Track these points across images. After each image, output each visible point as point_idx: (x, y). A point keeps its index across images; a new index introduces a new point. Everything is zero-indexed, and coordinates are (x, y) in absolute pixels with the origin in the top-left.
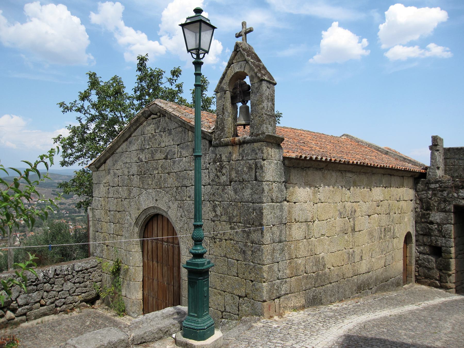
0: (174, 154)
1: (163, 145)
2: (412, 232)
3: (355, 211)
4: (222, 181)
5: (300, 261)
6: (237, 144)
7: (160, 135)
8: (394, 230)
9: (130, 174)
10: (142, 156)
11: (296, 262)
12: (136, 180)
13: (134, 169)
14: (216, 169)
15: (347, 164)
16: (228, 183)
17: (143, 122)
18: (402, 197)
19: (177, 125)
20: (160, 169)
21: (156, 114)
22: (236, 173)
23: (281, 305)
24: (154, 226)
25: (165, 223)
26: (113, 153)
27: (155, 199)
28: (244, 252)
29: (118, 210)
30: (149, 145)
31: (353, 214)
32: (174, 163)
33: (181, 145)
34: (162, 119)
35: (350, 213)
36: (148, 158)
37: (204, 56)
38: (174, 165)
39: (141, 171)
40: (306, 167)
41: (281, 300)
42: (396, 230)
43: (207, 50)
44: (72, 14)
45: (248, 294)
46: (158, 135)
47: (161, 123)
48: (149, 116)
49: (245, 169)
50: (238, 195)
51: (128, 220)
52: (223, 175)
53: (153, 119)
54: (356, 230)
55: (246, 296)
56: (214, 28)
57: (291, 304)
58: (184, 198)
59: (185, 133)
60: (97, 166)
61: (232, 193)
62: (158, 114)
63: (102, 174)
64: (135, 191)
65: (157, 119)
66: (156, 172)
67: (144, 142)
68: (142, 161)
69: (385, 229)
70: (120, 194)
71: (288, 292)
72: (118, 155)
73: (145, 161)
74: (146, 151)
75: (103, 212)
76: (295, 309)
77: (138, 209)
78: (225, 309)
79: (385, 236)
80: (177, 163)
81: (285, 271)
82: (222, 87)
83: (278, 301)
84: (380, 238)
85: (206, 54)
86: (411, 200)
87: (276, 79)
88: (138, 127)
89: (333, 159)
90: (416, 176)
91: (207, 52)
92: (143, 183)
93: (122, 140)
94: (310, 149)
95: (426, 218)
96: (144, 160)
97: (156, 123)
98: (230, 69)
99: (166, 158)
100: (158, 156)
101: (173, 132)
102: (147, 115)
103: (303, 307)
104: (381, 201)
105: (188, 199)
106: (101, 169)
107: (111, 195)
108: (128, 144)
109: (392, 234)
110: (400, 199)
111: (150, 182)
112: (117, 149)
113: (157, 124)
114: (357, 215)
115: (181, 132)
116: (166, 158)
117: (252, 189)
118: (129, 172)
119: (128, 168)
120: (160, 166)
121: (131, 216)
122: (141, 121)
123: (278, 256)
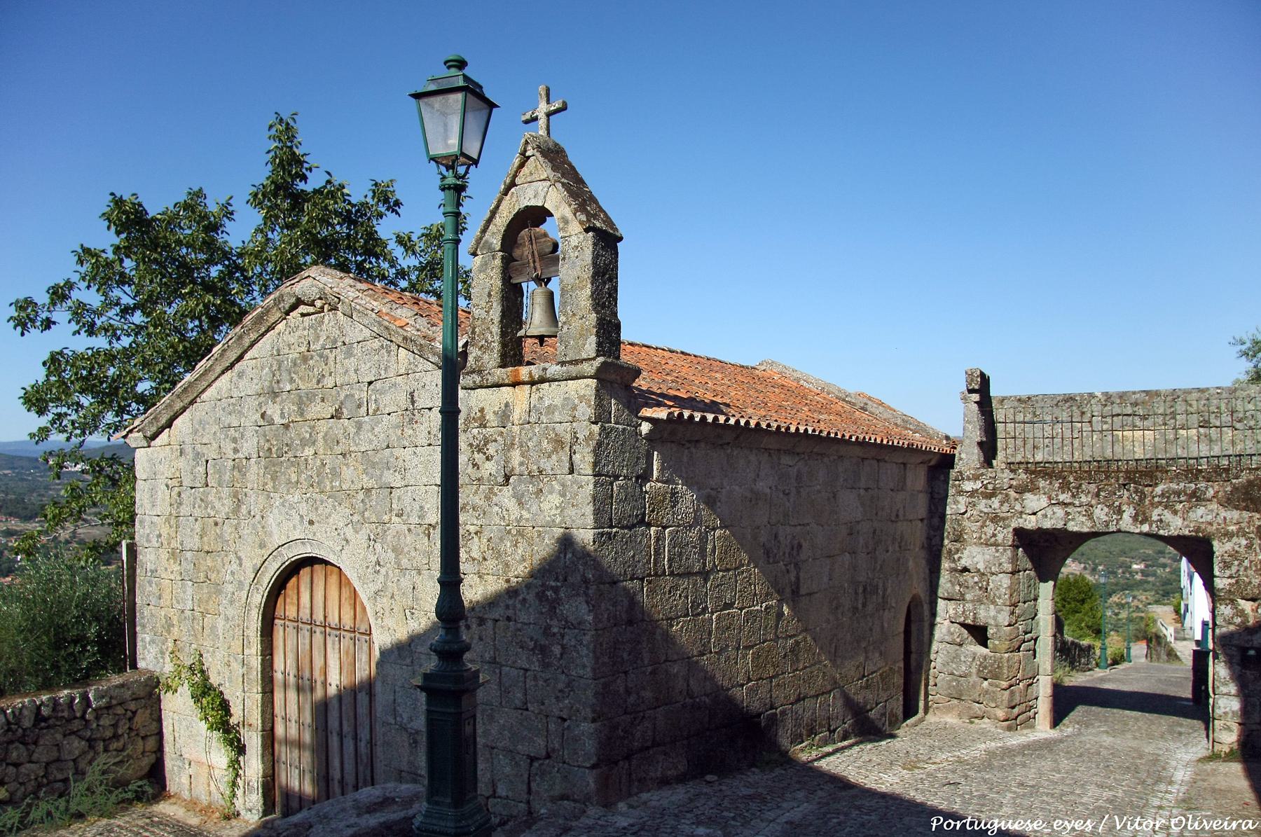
0: (359, 406)
1: (329, 382)
2: (922, 595)
3: (800, 546)
4: (486, 475)
5: (675, 669)
6: (524, 383)
7: (321, 356)
8: (885, 590)
9: (240, 455)
10: (273, 410)
11: (666, 671)
12: (254, 471)
13: (249, 446)
14: (471, 445)
15: (781, 435)
16: (500, 479)
17: (276, 323)
18: (901, 513)
19: (367, 333)
20: (320, 442)
21: (312, 304)
22: (522, 455)
23: (634, 776)
24: (302, 589)
25: (333, 580)
26: (192, 402)
27: (306, 519)
28: (543, 650)
29: (206, 548)
30: (292, 381)
31: (795, 553)
32: (359, 426)
33: (378, 385)
34: (328, 317)
35: (787, 551)
36: (290, 415)
37: (467, 172)
38: (357, 433)
39: (270, 449)
40: (689, 442)
41: (634, 762)
42: (889, 590)
43: (475, 157)
44: (543, 207)
45: (554, 750)
46: (317, 358)
47: (324, 327)
48: (294, 307)
49: (545, 444)
50: (528, 510)
51: (233, 573)
52: (487, 459)
53: (303, 315)
54: (803, 591)
55: (548, 756)
56: (492, 106)
57: (656, 770)
58: (386, 518)
59: (389, 352)
60: (149, 434)
61: (511, 504)
62: (319, 303)
63: (162, 456)
64: (254, 502)
65: (313, 317)
66: (309, 452)
67: (277, 373)
68: (272, 423)
69: (865, 590)
70: (213, 508)
71: (649, 744)
72: (206, 406)
73: (284, 421)
74: (284, 396)
75: (164, 555)
76: (664, 782)
77: (262, 545)
78: (494, 791)
79: (864, 605)
80: (366, 427)
81: (643, 693)
82: (486, 242)
83: (627, 766)
84: (855, 609)
85: (473, 168)
86: (922, 520)
87: (622, 230)
88: (263, 335)
89: (753, 424)
90: (932, 463)
91: (476, 162)
92: (274, 479)
93: (218, 369)
94: (287, 364)
95: (954, 561)
96: (278, 420)
97: (311, 327)
98: (508, 197)
99: (336, 416)
100: (317, 409)
101: (357, 350)
102: (287, 307)
103: (682, 779)
104: (858, 522)
105: (394, 519)
106: (158, 441)
107: (185, 510)
108: (235, 379)
109: (880, 600)
110: (897, 516)
111: (294, 478)
112: (203, 391)
113: (316, 330)
114: (803, 556)
115: (377, 351)
116: (336, 416)
117: (563, 495)
118: (236, 451)
119: (235, 440)
120: (321, 435)
121: (241, 565)
122: (272, 320)
123: (625, 656)
